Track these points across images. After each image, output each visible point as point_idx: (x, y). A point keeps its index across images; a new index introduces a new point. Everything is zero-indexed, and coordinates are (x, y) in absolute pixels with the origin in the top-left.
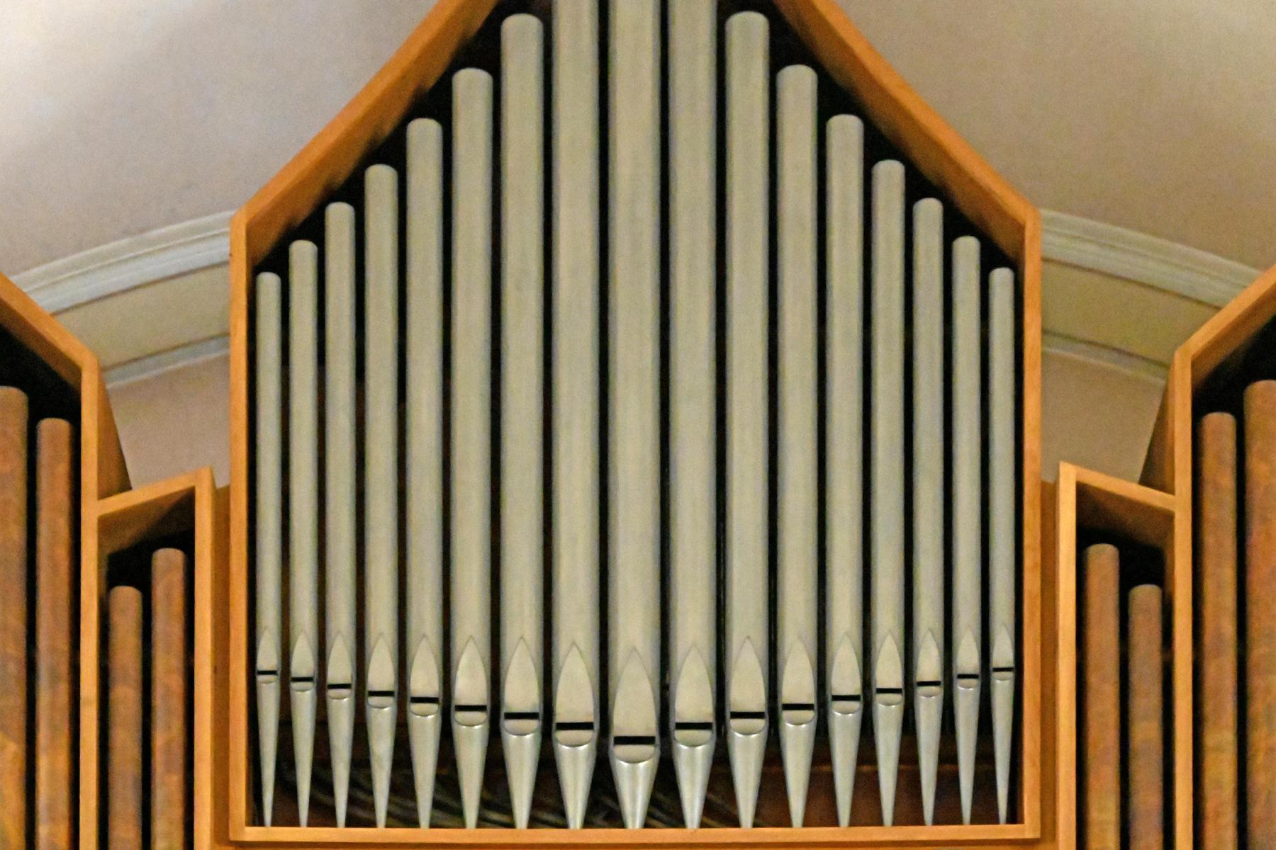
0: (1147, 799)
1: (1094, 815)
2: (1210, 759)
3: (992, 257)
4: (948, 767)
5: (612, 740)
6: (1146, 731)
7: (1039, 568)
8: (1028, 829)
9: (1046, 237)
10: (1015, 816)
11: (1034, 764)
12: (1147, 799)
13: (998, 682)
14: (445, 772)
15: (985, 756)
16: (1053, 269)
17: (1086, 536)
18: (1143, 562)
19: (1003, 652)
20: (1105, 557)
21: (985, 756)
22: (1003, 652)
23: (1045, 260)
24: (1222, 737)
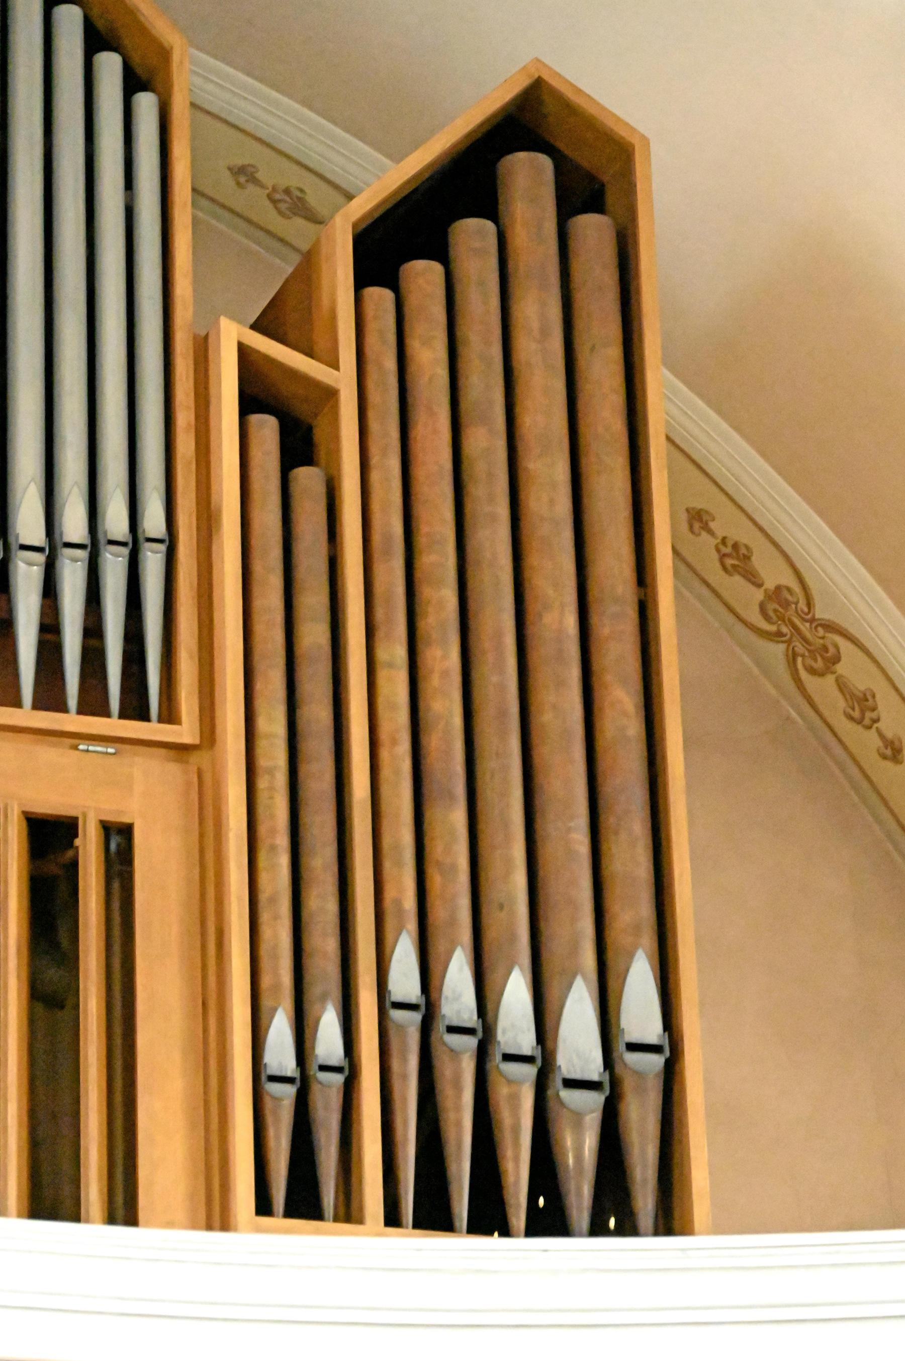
0: (317, 713)
1: (262, 724)
2: (382, 675)
3: (133, 83)
4: (93, 642)
5: (498, 1057)
6: (314, 634)
7: (193, 430)
8: (185, 732)
9: (195, 74)
10: (169, 716)
11: (191, 657)
12: (317, 713)
13: (108, 555)
14: (48, 621)
15: (93, 631)
16: (200, 115)
17: (250, 403)
18: (300, 446)
19: (154, 520)
20: (266, 428)
21: (93, 631)
22: (154, 520)
23: (193, 105)
24: (394, 651)
